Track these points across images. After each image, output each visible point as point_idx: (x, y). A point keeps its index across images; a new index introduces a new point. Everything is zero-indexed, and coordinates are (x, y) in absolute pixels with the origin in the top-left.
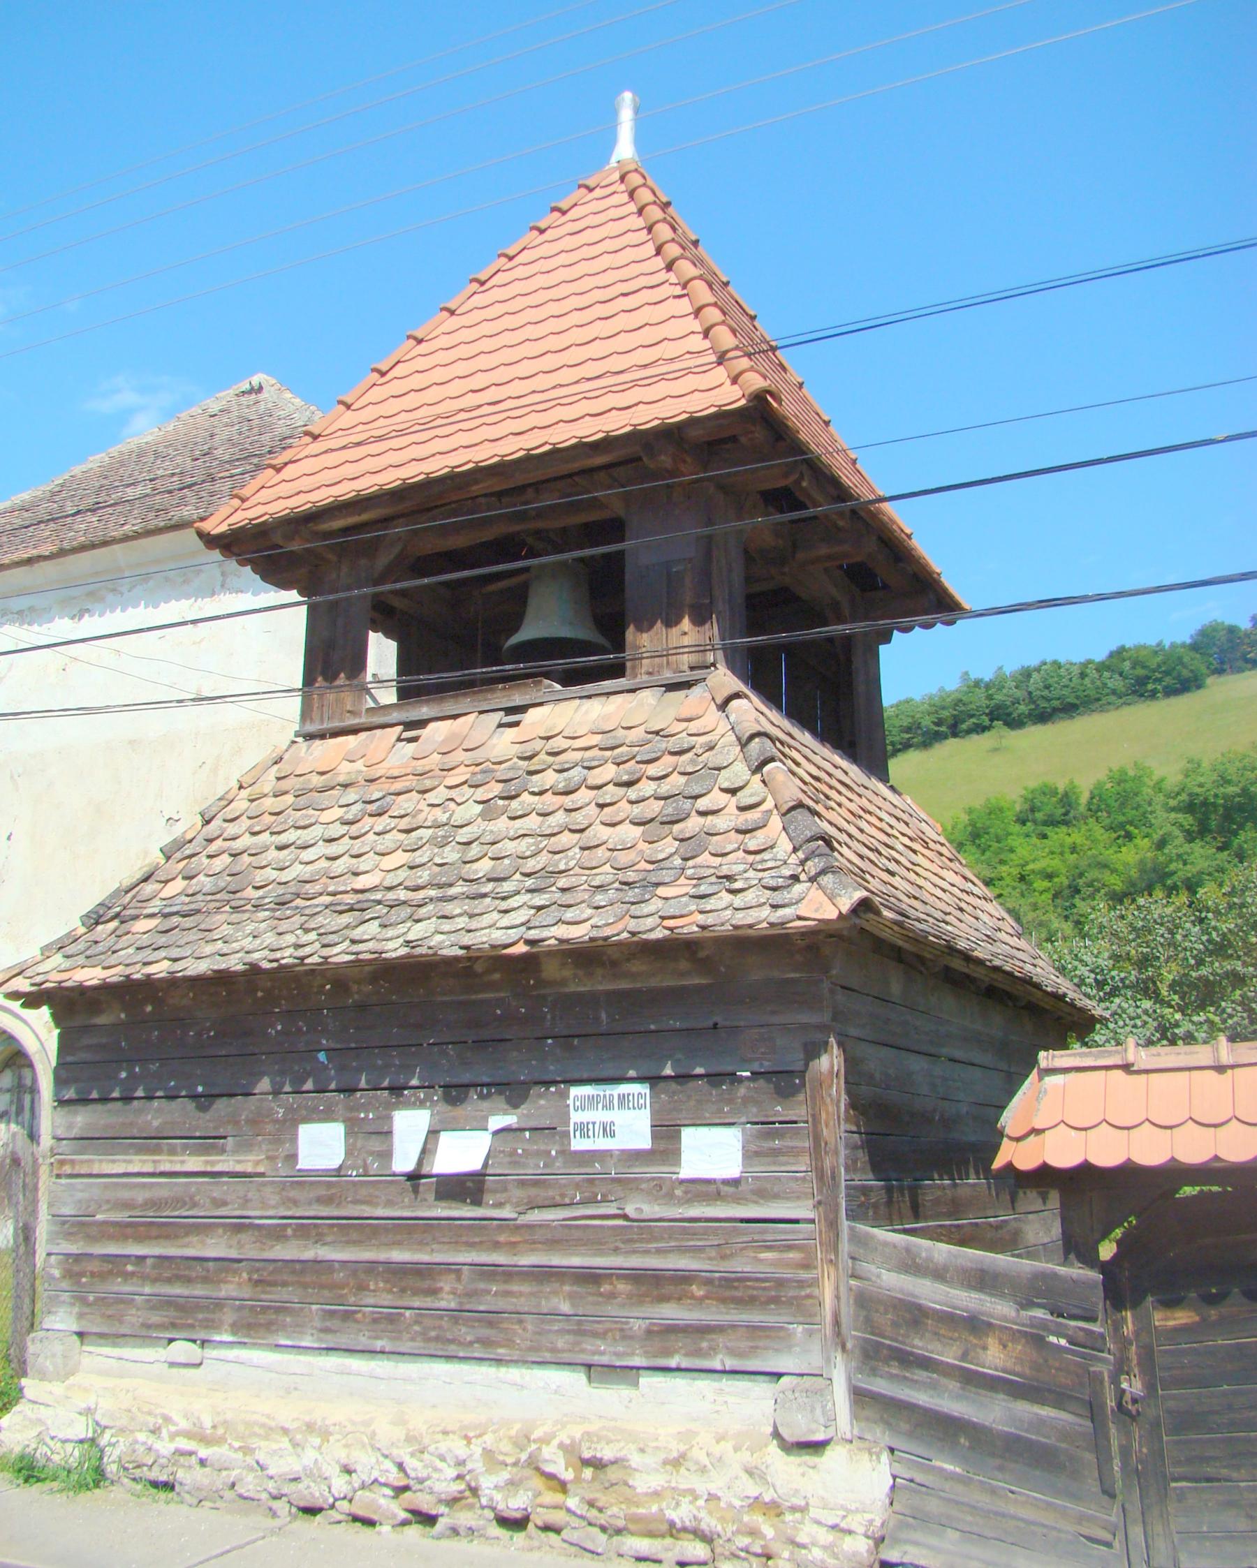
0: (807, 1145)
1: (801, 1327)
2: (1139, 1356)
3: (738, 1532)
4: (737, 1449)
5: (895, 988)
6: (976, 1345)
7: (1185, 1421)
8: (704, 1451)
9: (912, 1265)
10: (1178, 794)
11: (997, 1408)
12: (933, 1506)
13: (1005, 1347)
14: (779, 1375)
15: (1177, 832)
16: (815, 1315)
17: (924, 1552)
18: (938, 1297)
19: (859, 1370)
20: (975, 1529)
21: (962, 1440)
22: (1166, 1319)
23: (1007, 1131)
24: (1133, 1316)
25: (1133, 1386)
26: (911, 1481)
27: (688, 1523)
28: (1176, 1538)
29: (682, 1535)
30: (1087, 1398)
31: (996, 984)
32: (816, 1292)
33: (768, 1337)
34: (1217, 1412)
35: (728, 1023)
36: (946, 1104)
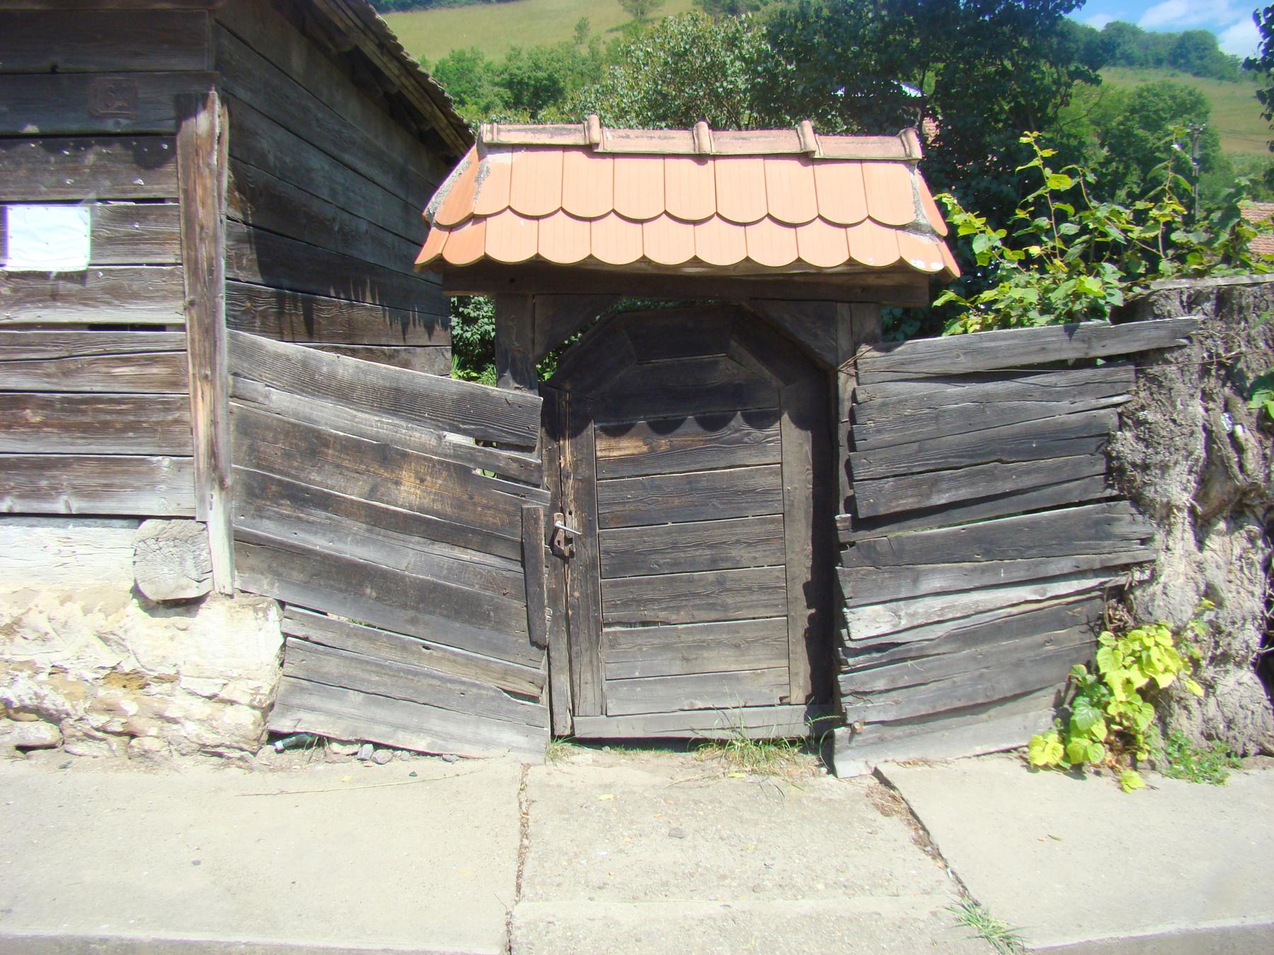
0: (176, 230)
1: (167, 460)
2: (577, 491)
3: (92, 709)
4: (87, 611)
5: (297, 63)
6: (387, 479)
8: (44, 616)
9: (315, 384)
10: (502, 73)
11: (411, 553)
12: (332, 666)
13: (422, 481)
14: (142, 518)
15: (498, 101)
16: (185, 445)
17: (322, 718)
18: (341, 422)
19: (242, 511)
20: (382, 690)
21: (368, 591)
22: (609, 449)
23: (437, 218)
25: (569, 524)
26: (306, 639)
27: (28, 702)
28: (605, 685)
29: (22, 715)
31: (405, 92)
32: (187, 416)
33: (125, 472)
34: (656, 552)
35: (71, 66)
36: (346, 216)
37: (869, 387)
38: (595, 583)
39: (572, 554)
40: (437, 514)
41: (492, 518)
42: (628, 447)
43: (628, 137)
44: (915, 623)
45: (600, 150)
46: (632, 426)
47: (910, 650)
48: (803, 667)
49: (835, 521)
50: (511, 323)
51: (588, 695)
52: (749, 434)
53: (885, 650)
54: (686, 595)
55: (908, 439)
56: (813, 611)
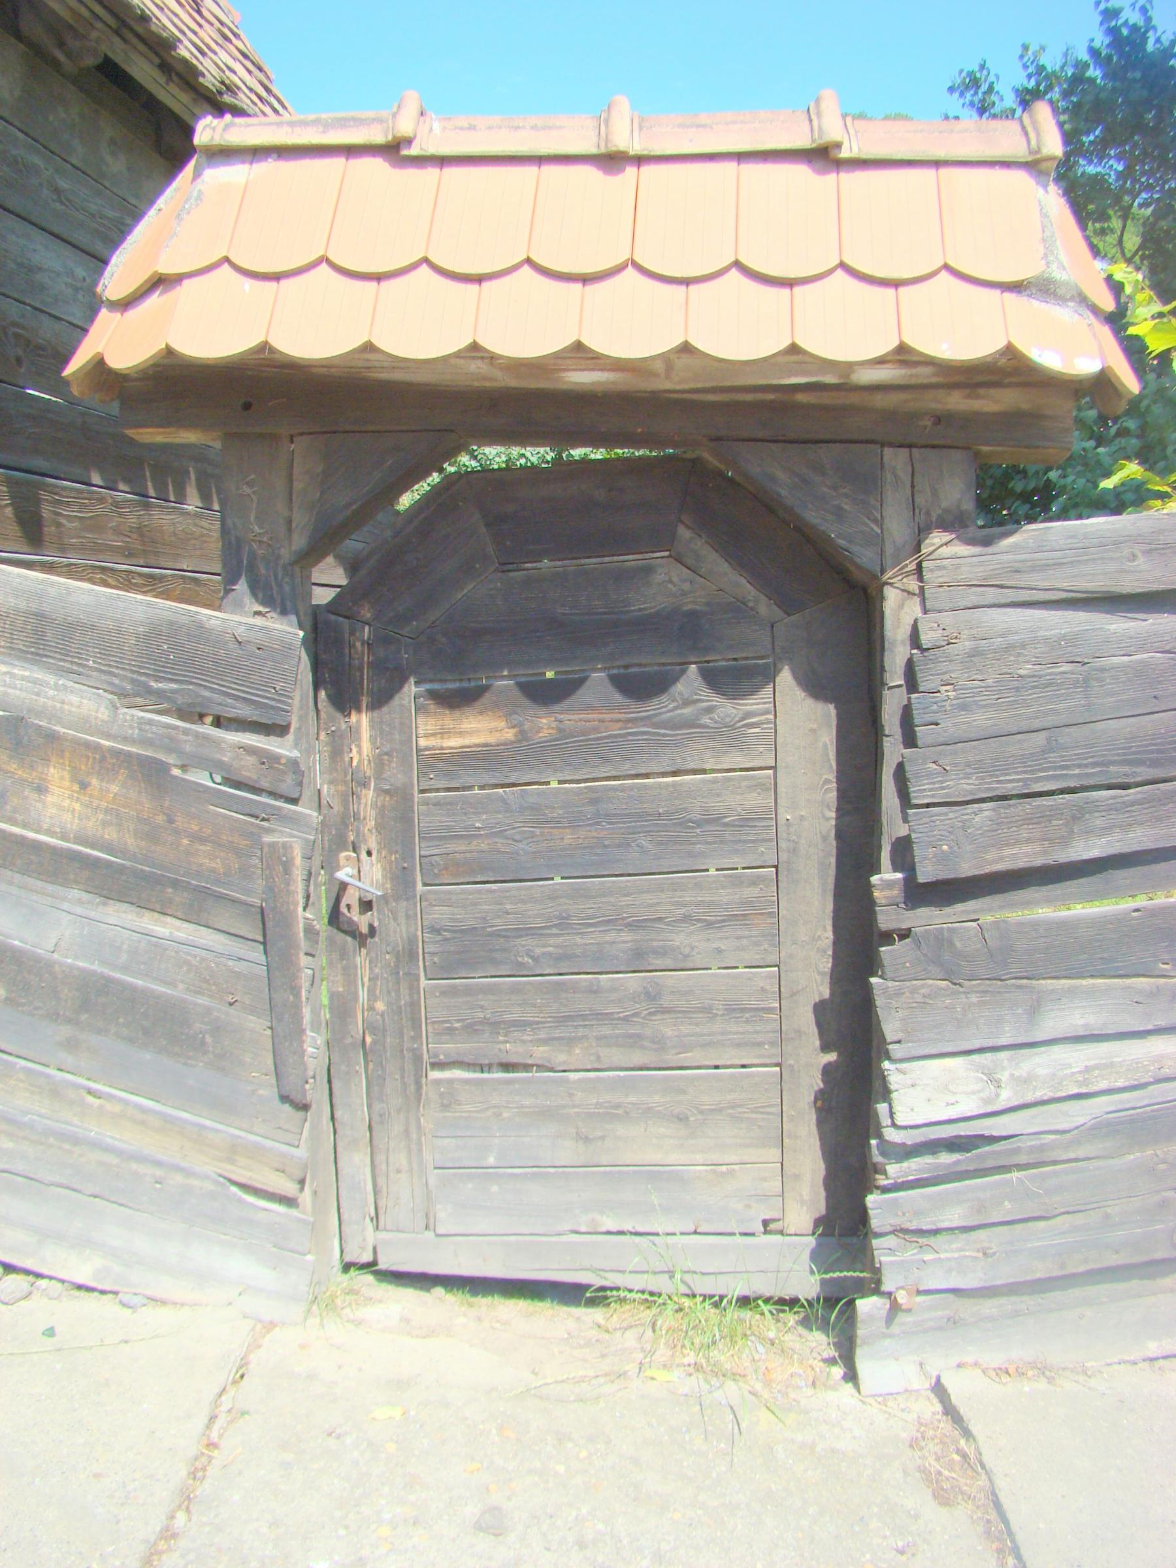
2: (381, 811)
7: (468, 950)
13: (84, 786)
20: (20, 1166)
22: (442, 734)
24: (372, 724)
30: (257, 902)
37: (946, 618)
38: (414, 988)
39: (372, 931)
40: (109, 848)
41: (208, 859)
42: (477, 729)
43: (472, 128)
44: (1029, 1097)
45: (414, 151)
46: (484, 689)
47: (1017, 1151)
48: (810, 1165)
49: (869, 887)
50: (247, 490)
51: (403, 1192)
52: (710, 710)
53: (964, 1147)
54: (584, 1017)
55: (1024, 726)
56: (832, 1057)
